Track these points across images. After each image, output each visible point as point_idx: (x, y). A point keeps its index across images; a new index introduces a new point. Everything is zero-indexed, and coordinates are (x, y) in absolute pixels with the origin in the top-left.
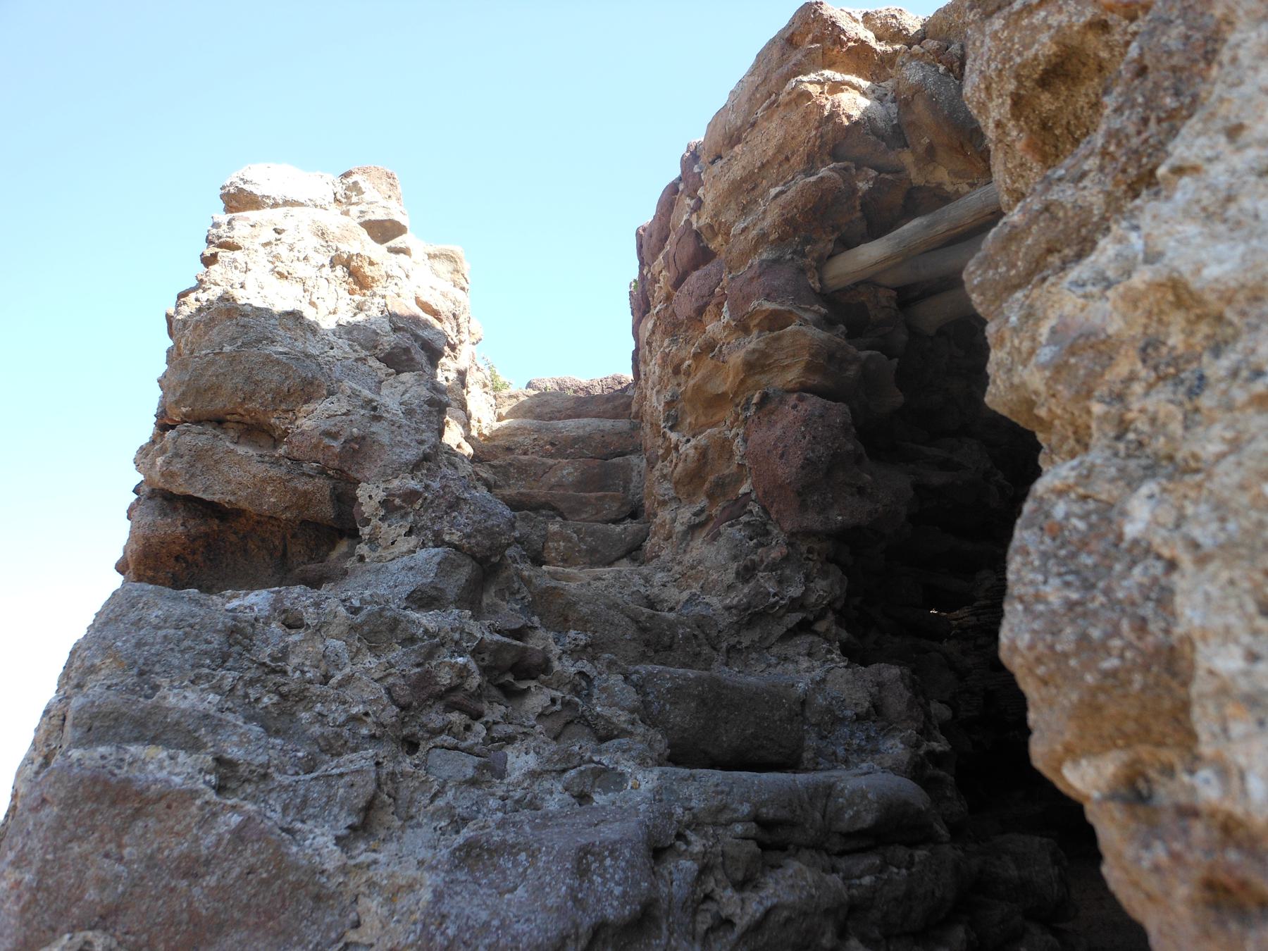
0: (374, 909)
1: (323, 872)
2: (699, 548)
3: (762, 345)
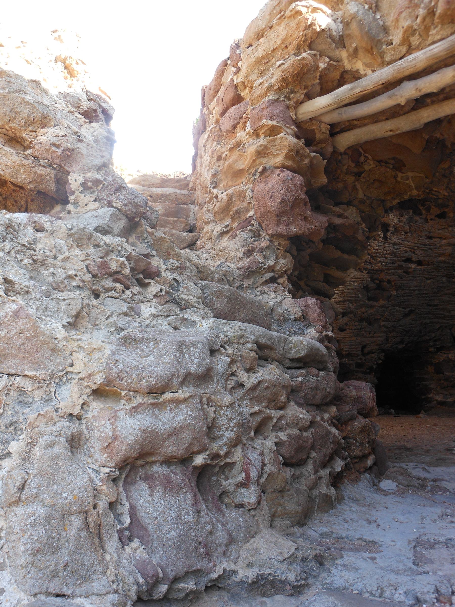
0: (80, 358)
1: (56, 339)
2: (226, 242)
3: (265, 143)
